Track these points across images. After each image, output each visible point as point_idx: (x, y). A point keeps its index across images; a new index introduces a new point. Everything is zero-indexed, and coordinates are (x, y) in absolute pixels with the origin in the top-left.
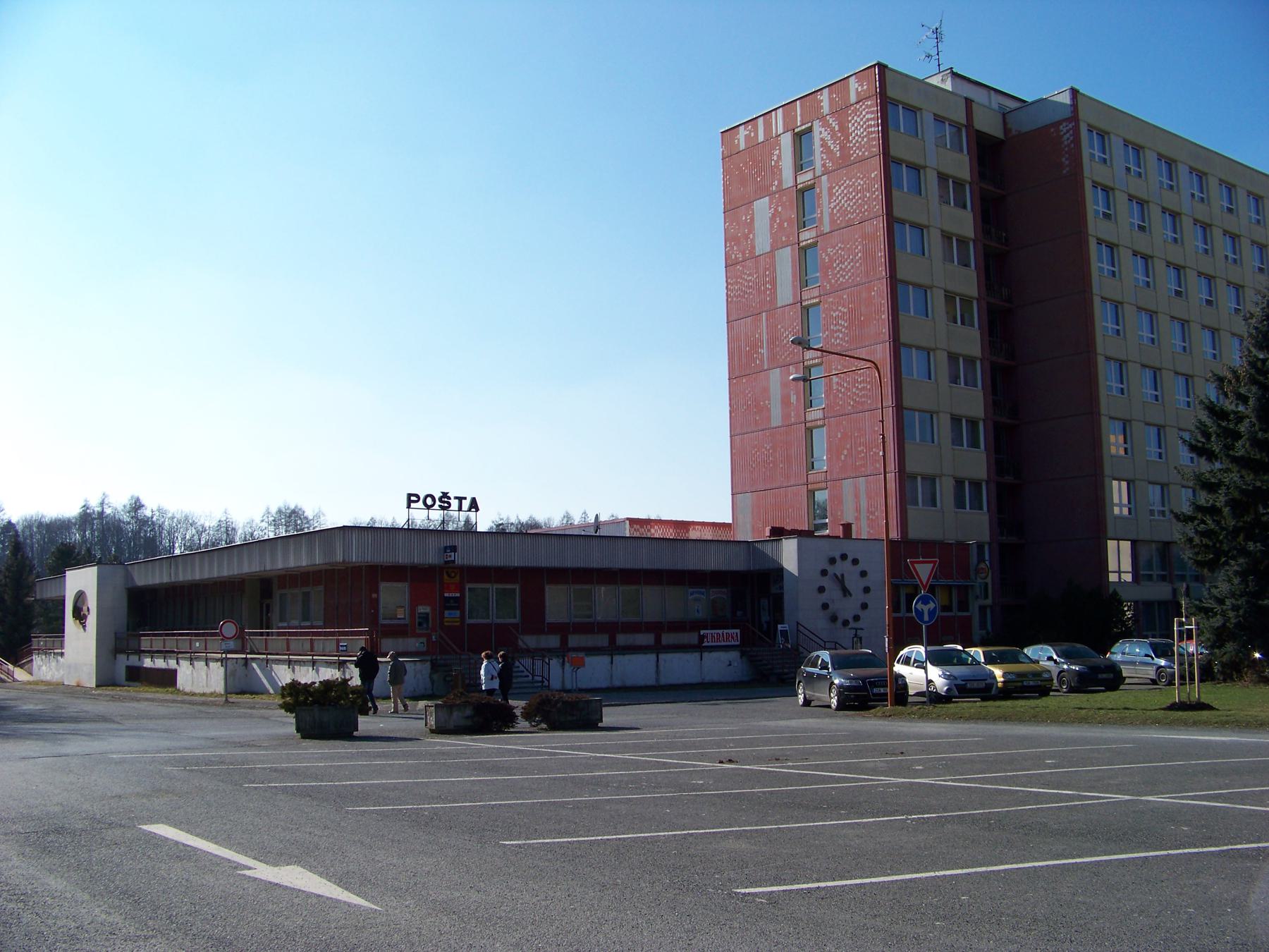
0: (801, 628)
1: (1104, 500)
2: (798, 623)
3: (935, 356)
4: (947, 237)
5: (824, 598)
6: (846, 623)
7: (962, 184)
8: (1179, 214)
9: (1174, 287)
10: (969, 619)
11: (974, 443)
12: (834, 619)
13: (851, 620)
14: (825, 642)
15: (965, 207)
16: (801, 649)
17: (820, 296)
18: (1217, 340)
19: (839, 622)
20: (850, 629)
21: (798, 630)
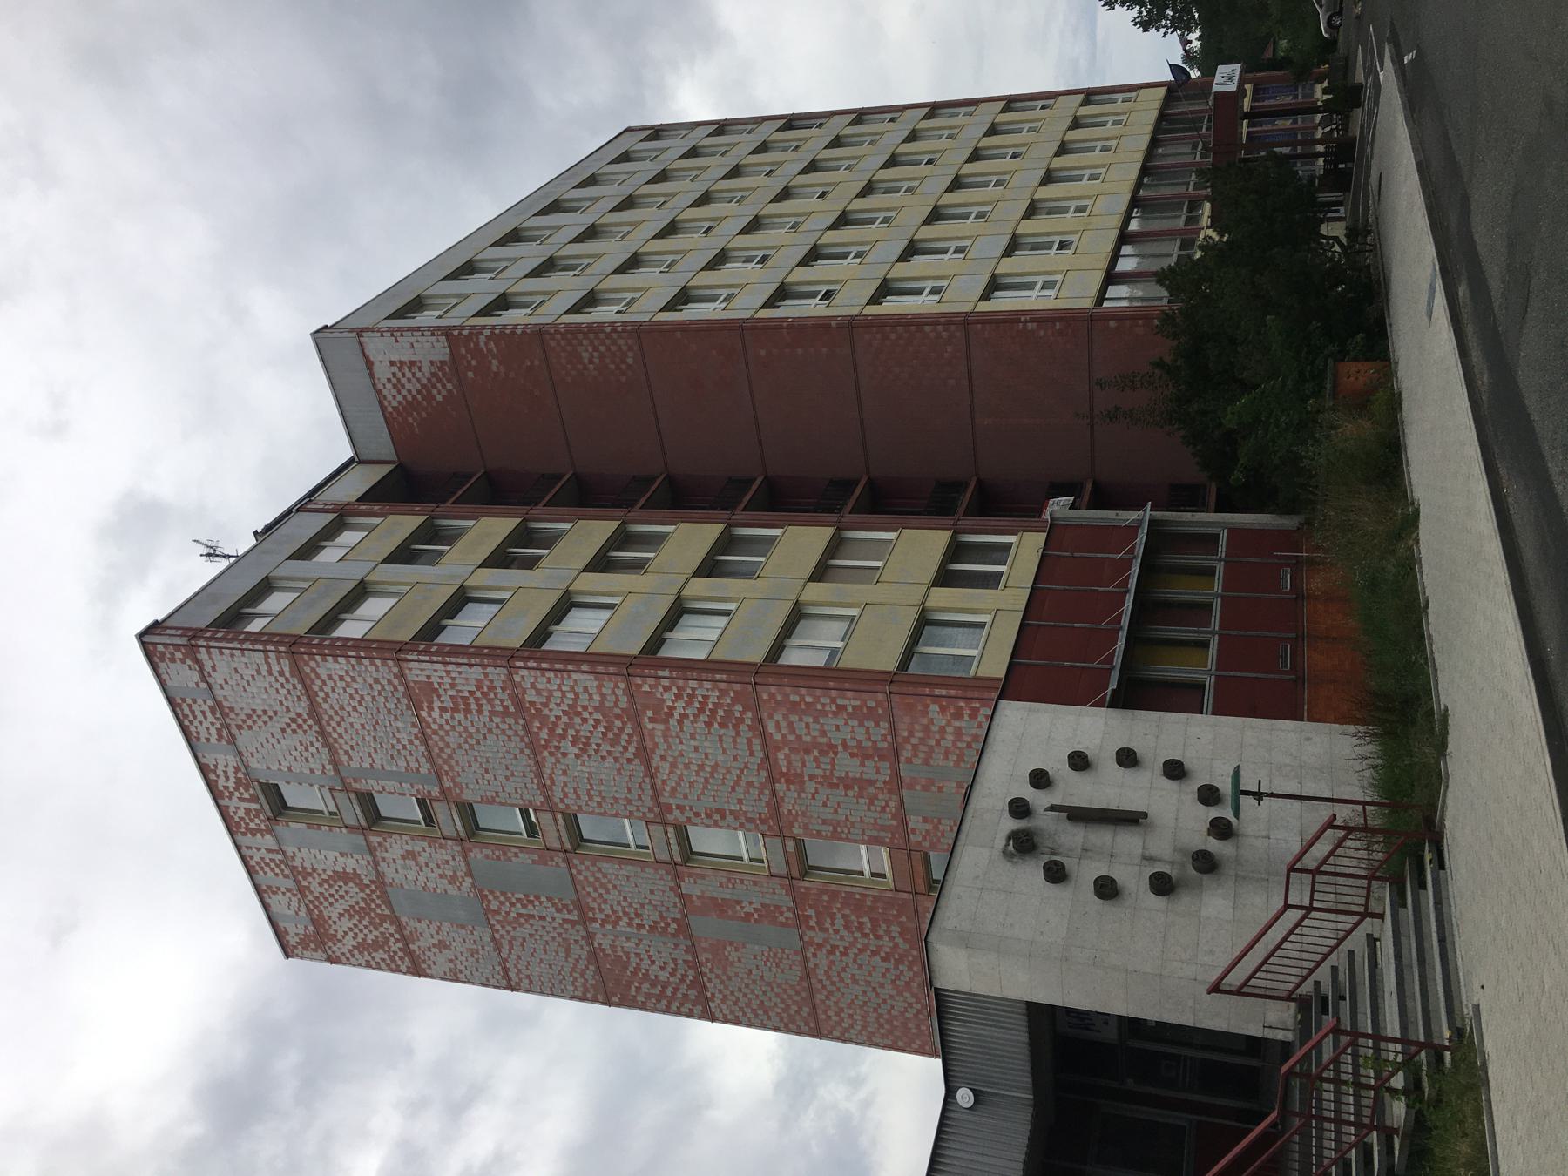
0: (1235, 979)
1: (1387, 294)
2: (1216, 988)
3: (814, 604)
4: (944, 578)
5: (1132, 879)
6: (1221, 829)
7: (957, 546)
8: (885, 281)
9: (1054, 251)
10: (1234, 532)
11: (654, 541)
12: (1206, 863)
13: (1214, 812)
14: (1287, 906)
15: (539, 558)
16: (1307, 988)
17: (553, 812)
18: (933, 245)
19: (1214, 845)
20: (1237, 815)
21: (1239, 992)
